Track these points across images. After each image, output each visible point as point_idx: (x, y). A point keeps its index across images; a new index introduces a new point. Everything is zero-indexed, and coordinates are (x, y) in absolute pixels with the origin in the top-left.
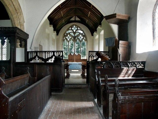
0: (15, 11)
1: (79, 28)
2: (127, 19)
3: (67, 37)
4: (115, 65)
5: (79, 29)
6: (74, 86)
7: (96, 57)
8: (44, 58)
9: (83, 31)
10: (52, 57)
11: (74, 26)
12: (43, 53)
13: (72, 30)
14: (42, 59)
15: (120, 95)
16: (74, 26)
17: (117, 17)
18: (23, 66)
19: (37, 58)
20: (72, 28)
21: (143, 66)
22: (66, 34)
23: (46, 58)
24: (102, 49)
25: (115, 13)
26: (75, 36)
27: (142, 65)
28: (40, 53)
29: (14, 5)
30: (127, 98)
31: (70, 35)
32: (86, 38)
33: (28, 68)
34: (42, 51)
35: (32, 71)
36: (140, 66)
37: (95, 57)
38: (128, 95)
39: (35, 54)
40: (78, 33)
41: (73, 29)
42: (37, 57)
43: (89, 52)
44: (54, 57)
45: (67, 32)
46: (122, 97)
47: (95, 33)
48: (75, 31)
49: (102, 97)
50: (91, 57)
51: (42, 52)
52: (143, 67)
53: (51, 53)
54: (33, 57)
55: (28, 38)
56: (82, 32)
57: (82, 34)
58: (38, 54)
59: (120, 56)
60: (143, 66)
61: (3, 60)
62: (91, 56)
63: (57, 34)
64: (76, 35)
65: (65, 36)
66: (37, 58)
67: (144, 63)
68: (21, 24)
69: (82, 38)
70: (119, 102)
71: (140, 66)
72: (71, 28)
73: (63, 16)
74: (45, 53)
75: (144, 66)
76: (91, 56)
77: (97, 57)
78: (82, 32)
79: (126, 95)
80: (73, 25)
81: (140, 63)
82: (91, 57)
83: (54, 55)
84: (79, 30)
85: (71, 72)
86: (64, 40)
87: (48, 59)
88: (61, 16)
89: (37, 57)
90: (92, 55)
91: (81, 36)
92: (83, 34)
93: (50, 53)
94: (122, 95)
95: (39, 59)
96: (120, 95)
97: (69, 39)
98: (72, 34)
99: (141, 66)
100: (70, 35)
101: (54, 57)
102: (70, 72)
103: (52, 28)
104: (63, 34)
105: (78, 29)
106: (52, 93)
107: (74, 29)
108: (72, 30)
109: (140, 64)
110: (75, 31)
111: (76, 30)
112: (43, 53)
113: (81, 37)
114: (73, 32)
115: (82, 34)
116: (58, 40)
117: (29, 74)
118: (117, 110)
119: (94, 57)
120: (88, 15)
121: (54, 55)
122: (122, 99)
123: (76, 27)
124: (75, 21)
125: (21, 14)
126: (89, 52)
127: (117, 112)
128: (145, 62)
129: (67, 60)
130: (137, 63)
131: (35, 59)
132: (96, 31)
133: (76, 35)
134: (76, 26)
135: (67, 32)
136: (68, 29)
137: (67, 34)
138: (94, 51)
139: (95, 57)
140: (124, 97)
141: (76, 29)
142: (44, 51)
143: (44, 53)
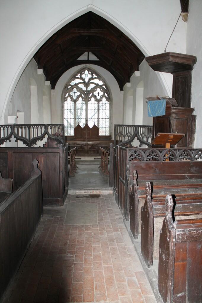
1: (96, 74)
3: (72, 93)
5: (96, 77)
6: (85, 191)
9: (104, 81)
10: (41, 138)
11: (86, 72)
13: (81, 78)
15: (174, 228)
16: (86, 72)
22: (69, 87)
23: (32, 137)
24: (140, 122)
26: (88, 91)
30: (187, 233)
31: (78, 88)
35: (4, 165)
38: (190, 227)
39: (10, 131)
40: (94, 85)
41: (83, 76)
42: (13, 136)
43: (115, 125)
44: (47, 136)
45: (73, 83)
46: (178, 231)
48: (87, 80)
49: (132, 301)
54: (6, 135)
56: (101, 83)
57: (101, 86)
58: (16, 131)
64: (89, 89)
65: (67, 89)
66: (13, 139)
69: (102, 93)
70: (173, 241)
72: (79, 75)
74: (29, 129)
78: (101, 83)
79: (186, 227)
83: (46, 133)
84: (95, 78)
86: (64, 99)
87: (35, 140)
89: (13, 136)
90: (143, 133)
91: (98, 90)
93: (39, 128)
94: (178, 228)
96: (175, 226)
97: (76, 97)
98: (81, 86)
100: (78, 88)
101: (47, 136)
102: (79, 162)
105: (94, 77)
106: (44, 207)
107: (87, 75)
108: (81, 78)
110: (87, 80)
111: (90, 79)
113: (99, 93)
115: (101, 87)
118: (168, 254)
119: (124, 136)
121: (46, 133)
122: (179, 235)
123: (90, 73)
124: (88, 62)
126: (115, 125)
127: (168, 259)
131: (10, 141)
133: (89, 89)
134: (89, 70)
135: (73, 83)
136: (74, 77)
138: (124, 124)
140: (183, 231)
141: (90, 76)
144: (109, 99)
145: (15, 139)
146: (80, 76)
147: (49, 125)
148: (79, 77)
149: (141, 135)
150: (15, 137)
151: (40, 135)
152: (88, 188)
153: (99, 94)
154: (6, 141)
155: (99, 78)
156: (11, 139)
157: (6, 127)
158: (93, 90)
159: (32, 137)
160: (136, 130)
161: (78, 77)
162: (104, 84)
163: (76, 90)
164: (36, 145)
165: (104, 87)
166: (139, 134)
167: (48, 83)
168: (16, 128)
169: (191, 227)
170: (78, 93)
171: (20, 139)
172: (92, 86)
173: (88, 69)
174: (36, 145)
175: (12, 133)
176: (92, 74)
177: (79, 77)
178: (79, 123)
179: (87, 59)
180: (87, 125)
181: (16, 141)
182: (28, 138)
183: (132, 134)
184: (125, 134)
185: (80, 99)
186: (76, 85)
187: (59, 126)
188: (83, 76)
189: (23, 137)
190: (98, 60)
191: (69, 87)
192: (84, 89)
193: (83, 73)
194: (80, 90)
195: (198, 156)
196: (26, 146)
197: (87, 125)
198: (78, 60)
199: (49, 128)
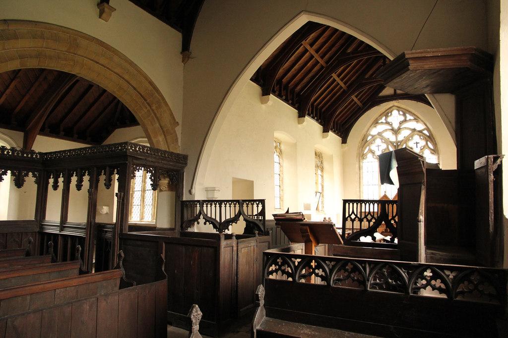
7: (369, 221)
10: (235, 220)
11: (395, 112)
13: (387, 123)
16: (395, 112)
20: (387, 116)
23: (223, 220)
32: (435, 144)
37: (365, 220)
41: (389, 119)
45: (374, 131)
50: (353, 220)
53: (235, 207)
54: (233, 215)
56: (420, 126)
57: (421, 132)
60: (441, 291)
61: (135, 218)
62: (350, 216)
63: (344, 141)
66: (202, 220)
68: (165, 129)
71: (429, 288)
74: (220, 207)
76: (350, 216)
77: (371, 220)
78: (420, 126)
80: (391, 107)
82: (353, 220)
89: (202, 217)
90: (353, 212)
91: (416, 138)
92: (426, 132)
100: (382, 138)
103: (311, 125)
104: (360, 139)
105: (408, 119)
107: (396, 118)
108: (387, 123)
111: (401, 123)
112: (215, 204)
114: (392, 130)
117: (122, 271)
119: (361, 220)
123: (401, 113)
130: (333, 263)
134: (399, 109)
136: (376, 122)
137: (373, 136)
139: (365, 220)
141: (402, 118)
145: (204, 221)
146: (386, 119)
147: (244, 201)
148: (385, 122)
149: (393, 218)
153: (418, 144)
154: (231, 225)
155: (417, 119)
156: (199, 220)
157: (255, 203)
159: (223, 220)
161: (382, 122)
162: (425, 127)
163: (380, 141)
164: (228, 230)
165: (426, 132)
166: (390, 218)
168: (205, 205)
172: (404, 134)
173: (397, 108)
174: (228, 230)
175: (240, 213)
176: (404, 115)
177: (385, 122)
178: (385, 192)
181: (205, 224)
182: (218, 219)
184: (363, 216)
186: (380, 134)
187: (257, 202)
188: (389, 119)
189: (213, 219)
190: (381, 94)
191: (370, 138)
192: (392, 138)
193: (390, 114)
196: (217, 231)
199: (245, 205)
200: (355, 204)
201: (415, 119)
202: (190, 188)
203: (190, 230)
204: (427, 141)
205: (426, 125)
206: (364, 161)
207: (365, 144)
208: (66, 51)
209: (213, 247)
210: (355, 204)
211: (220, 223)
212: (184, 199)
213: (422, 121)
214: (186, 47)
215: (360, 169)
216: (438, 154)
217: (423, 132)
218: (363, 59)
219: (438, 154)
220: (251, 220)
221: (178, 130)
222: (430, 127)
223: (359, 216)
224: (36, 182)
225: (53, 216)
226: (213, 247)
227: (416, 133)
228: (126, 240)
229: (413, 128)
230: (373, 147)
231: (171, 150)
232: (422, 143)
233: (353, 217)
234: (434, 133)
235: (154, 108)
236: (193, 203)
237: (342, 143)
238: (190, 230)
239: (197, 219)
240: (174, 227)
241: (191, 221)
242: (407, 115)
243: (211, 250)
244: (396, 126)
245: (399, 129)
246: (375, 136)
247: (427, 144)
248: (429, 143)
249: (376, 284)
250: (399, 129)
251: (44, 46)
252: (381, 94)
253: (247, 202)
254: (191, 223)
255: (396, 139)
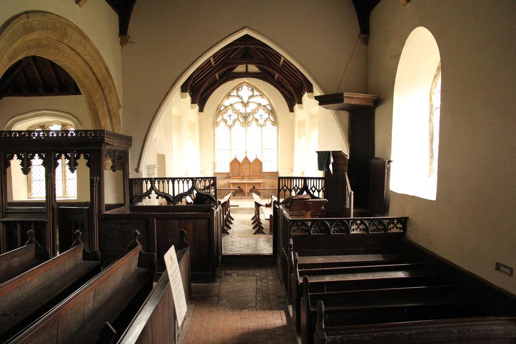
0: (96, 85)
2: (372, 104)
4: (334, 228)
7: (296, 191)
8: (171, 193)
11: (245, 88)
12: (168, 183)
13: (238, 96)
14: (166, 196)
16: (245, 88)
17: (346, 101)
18: (124, 221)
19: (153, 195)
20: (238, 90)
21: (400, 229)
23: (176, 194)
25: (339, 92)
26: (247, 113)
27: (399, 226)
28: (161, 182)
29: (94, 74)
32: (275, 118)
33: (136, 233)
34: (166, 179)
36: (395, 228)
39: (149, 185)
41: (240, 93)
45: (227, 103)
47: (297, 107)
51: (166, 180)
52: (402, 231)
55: (131, 145)
56: (264, 102)
57: (265, 106)
58: (156, 185)
59: (350, 197)
60: (400, 229)
61: (60, 196)
63: (201, 110)
64: (249, 109)
65: (219, 112)
66: (153, 195)
67: (404, 221)
68: (112, 112)
71: (395, 228)
73: (215, 63)
75: (404, 228)
76: (283, 188)
78: (264, 102)
80: (242, 83)
81: (395, 221)
82: (285, 191)
85: (238, 209)
86: (216, 124)
88: (211, 64)
89: (153, 192)
91: (261, 111)
95: (160, 197)
98: (239, 107)
99: (397, 228)
104: (216, 109)
107: (245, 92)
108: (238, 96)
109: (394, 224)
112: (168, 182)
113: (262, 115)
114: (242, 102)
116: (200, 123)
119: (291, 191)
120: (280, 61)
121: (193, 188)
123: (250, 89)
125: (111, 90)
128: (406, 219)
129: (226, 176)
131: (150, 198)
132: (300, 102)
133: (249, 110)
134: (248, 85)
137: (226, 107)
141: (250, 93)
142: (170, 179)
143: (170, 182)
144: (275, 123)
145: (157, 195)
146: (237, 93)
148: (236, 95)
149: (311, 188)
150: (156, 193)
151: (186, 190)
152: (279, 138)
154: (145, 198)
155: (262, 95)
156: (150, 195)
158: (254, 112)
160: (305, 183)
162: (269, 103)
165: (268, 107)
166: (309, 188)
167: (197, 107)
169: (343, 334)
170: (235, 116)
171: (161, 196)
172: (251, 107)
174: (182, 202)
176: (252, 90)
179: (230, 205)
180: (246, 158)
183: (300, 187)
185: (237, 123)
186: (231, 105)
188: (240, 93)
189: (166, 194)
191: (223, 108)
192: (242, 110)
193: (240, 89)
194: (238, 112)
195: (394, 225)
197: (246, 158)
198: (233, 73)
200: (320, 180)
201: (261, 95)
202: (136, 167)
203: (140, 204)
204: (269, 114)
205: (270, 102)
206: (217, 128)
207: (219, 113)
208: (57, 40)
209: (206, 218)
210: (320, 180)
211: (174, 197)
212: (131, 177)
213: (267, 98)
214: (123, 30)
215: (214, 136)
216: (278, 126)
217: (267, 107)
218: (238, 49)
219: (278, 126)
220: (205, 193)
221: (121, 112)
222: (273, 104)
223: (318, 188)
224: (44, 164)
225: (110, 197)
226: (206, 218)
227: (261, 107)
228: (104, 219)
229: (259, 103)
230: (226, 116)
231: (116, 132)
232: (266, 116)
233: (285, 188)
234: (276, 109)
235: (106, 92)
236: (140, 181)
237: (199, 112)
238: (140, 204)
239: (148, 194)
240: (123, 203)
241: (140, 196)
242: (255, 91)
243: (205, 221)
244: (245, 100)
245: (248, 103)
246: (227, 107)
247: (269, 117)
248: (270, 116)
249: (315, 231)
250: (248, 103)
251: (45, 36)
252: (235, 71)
253: (200, 179)
254: (142, 197)
255: (246, 111)
